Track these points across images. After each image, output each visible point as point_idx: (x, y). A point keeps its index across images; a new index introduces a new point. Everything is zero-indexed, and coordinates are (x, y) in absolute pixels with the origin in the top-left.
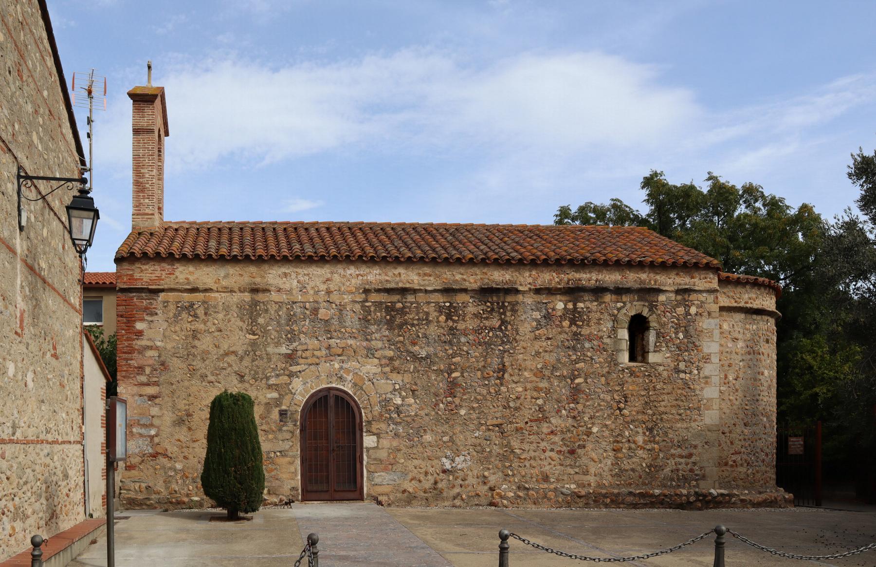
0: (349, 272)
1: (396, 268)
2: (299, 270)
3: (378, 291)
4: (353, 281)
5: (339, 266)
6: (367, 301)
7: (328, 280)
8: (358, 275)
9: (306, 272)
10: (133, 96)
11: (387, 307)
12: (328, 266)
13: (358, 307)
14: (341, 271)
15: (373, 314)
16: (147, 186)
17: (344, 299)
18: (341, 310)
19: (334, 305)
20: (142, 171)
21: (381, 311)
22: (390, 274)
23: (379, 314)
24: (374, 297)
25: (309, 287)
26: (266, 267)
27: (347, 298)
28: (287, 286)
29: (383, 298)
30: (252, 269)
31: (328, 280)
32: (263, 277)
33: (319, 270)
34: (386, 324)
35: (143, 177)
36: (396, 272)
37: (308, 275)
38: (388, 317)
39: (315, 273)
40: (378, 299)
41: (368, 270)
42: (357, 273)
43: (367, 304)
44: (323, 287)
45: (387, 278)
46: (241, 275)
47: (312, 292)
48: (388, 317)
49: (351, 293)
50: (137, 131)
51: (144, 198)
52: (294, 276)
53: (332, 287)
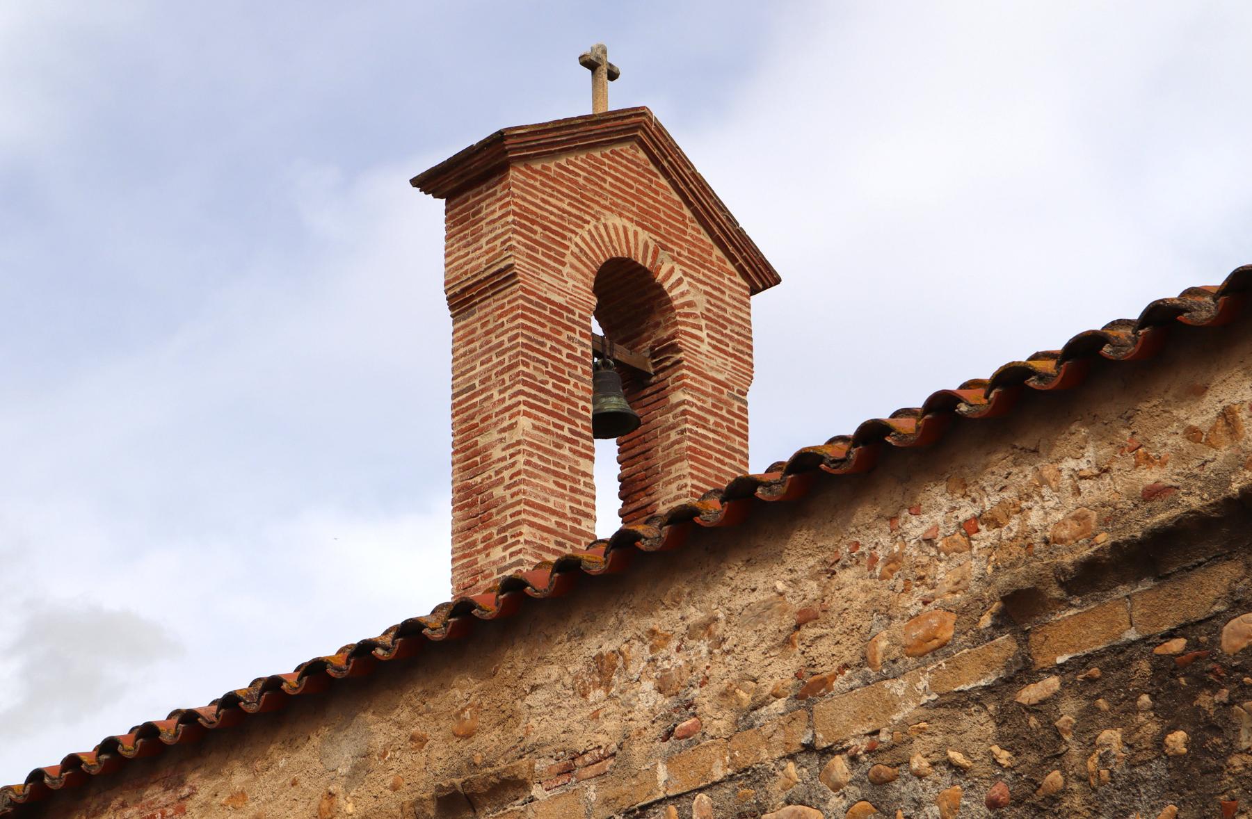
0: (915, 527)
1: (1199, 392)
2: (662, 620)
3: (1089, 578)
4: (943, 573)
5: (865, 513)
6: (1024, 672)
7: (805, 619)
8: (969, 528)
9: (695, 615)
10: (428, 182)
11: (1165, 669)
12: (801, 538)
13: (979, 726)
14: (881, 541)
15: (1074, 749)
16: (498, 492)
17: (891, 705)
18: (880, 783)
19: (839, 765)
20: (482, 441)
21: (1124, 713)
22: (1168, 440)
23: (1111, 737)
24: (1074, 631)
25: (704, 697)
26: (515, 660)
27: (910, 693)
28: (607, 733)
29: (1126, 615)
30: (463, 691)
31: (805, 619)
32: (507, 719)
33: (758, 577)
34: (1170, 789)
35: (486, 463)
36: (1203, 414)
37: (706, 626)
38: (1178, 740)
39: (739, 601)
40: (1094, 639)
41: (1025, 475)
42: (967, 511)
43: (1030, 694)
44: (781, 671)
45: (1151, 476)
46: (418, 741)
47: (720, 723)
48: (1178, 740)
49: (929, 650)
50: (462, 300)
51: (488, 544)
52: (639, 653)
53: (828, 650)
